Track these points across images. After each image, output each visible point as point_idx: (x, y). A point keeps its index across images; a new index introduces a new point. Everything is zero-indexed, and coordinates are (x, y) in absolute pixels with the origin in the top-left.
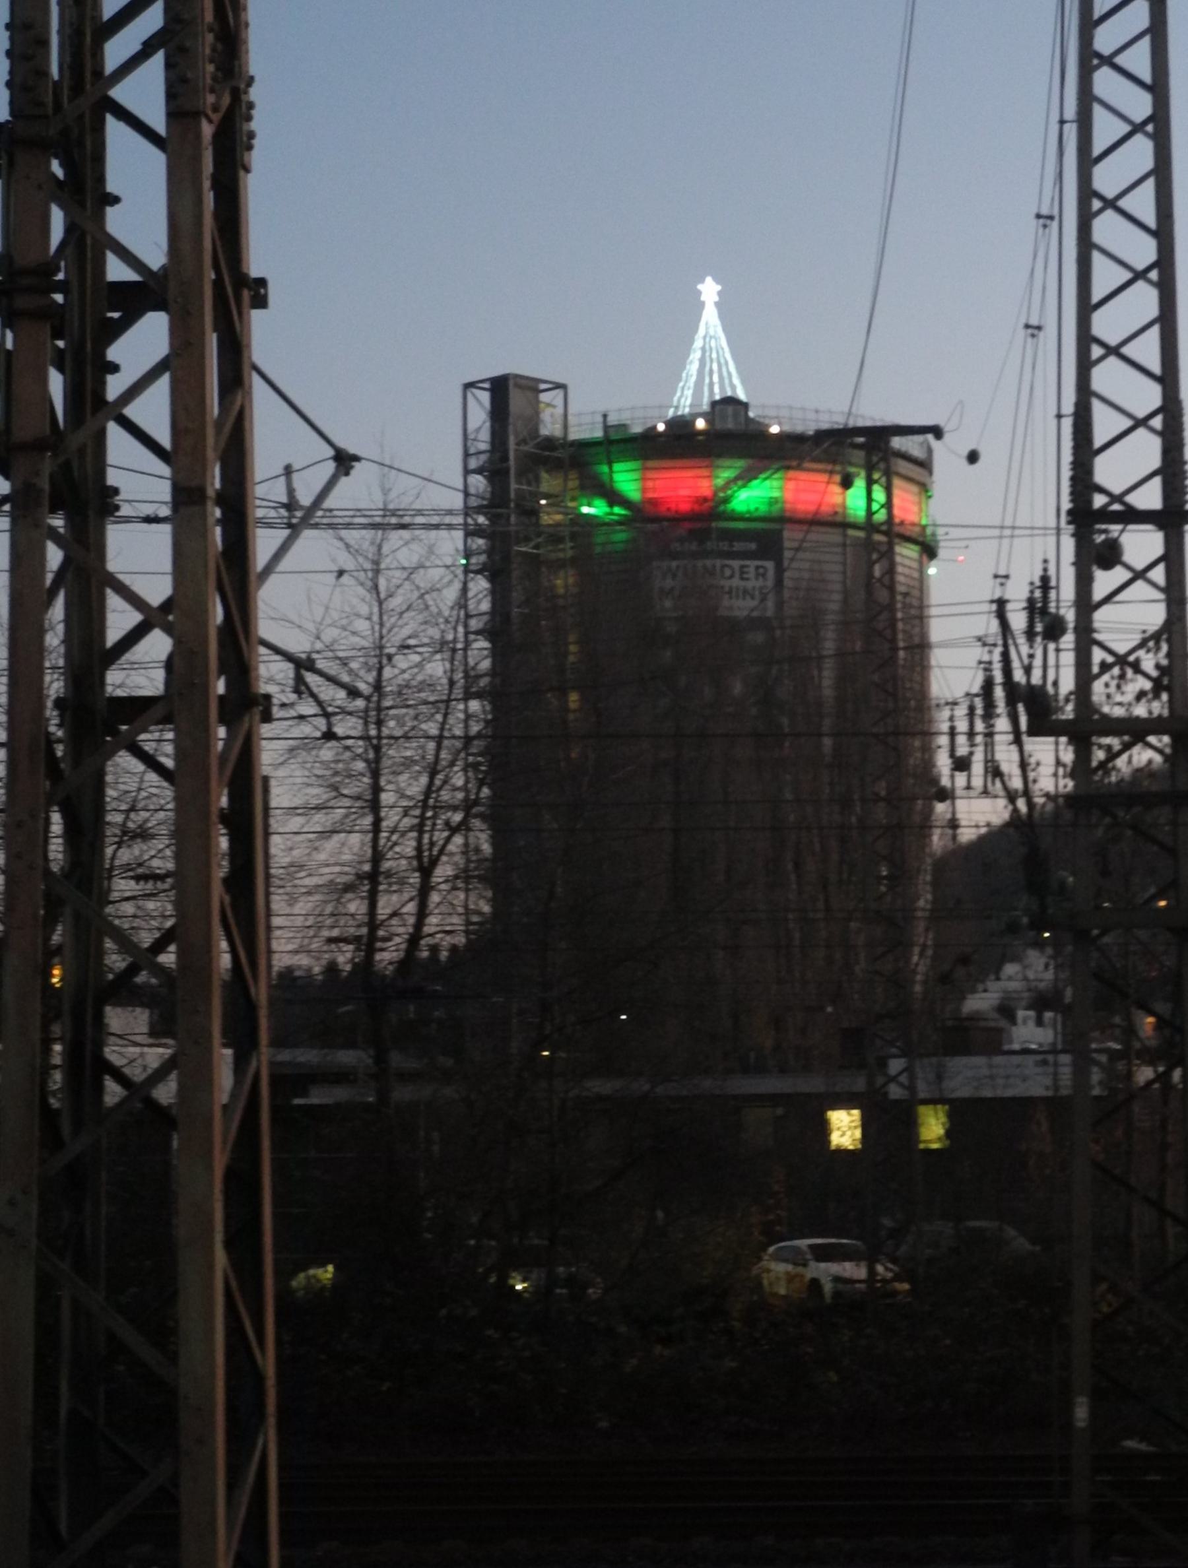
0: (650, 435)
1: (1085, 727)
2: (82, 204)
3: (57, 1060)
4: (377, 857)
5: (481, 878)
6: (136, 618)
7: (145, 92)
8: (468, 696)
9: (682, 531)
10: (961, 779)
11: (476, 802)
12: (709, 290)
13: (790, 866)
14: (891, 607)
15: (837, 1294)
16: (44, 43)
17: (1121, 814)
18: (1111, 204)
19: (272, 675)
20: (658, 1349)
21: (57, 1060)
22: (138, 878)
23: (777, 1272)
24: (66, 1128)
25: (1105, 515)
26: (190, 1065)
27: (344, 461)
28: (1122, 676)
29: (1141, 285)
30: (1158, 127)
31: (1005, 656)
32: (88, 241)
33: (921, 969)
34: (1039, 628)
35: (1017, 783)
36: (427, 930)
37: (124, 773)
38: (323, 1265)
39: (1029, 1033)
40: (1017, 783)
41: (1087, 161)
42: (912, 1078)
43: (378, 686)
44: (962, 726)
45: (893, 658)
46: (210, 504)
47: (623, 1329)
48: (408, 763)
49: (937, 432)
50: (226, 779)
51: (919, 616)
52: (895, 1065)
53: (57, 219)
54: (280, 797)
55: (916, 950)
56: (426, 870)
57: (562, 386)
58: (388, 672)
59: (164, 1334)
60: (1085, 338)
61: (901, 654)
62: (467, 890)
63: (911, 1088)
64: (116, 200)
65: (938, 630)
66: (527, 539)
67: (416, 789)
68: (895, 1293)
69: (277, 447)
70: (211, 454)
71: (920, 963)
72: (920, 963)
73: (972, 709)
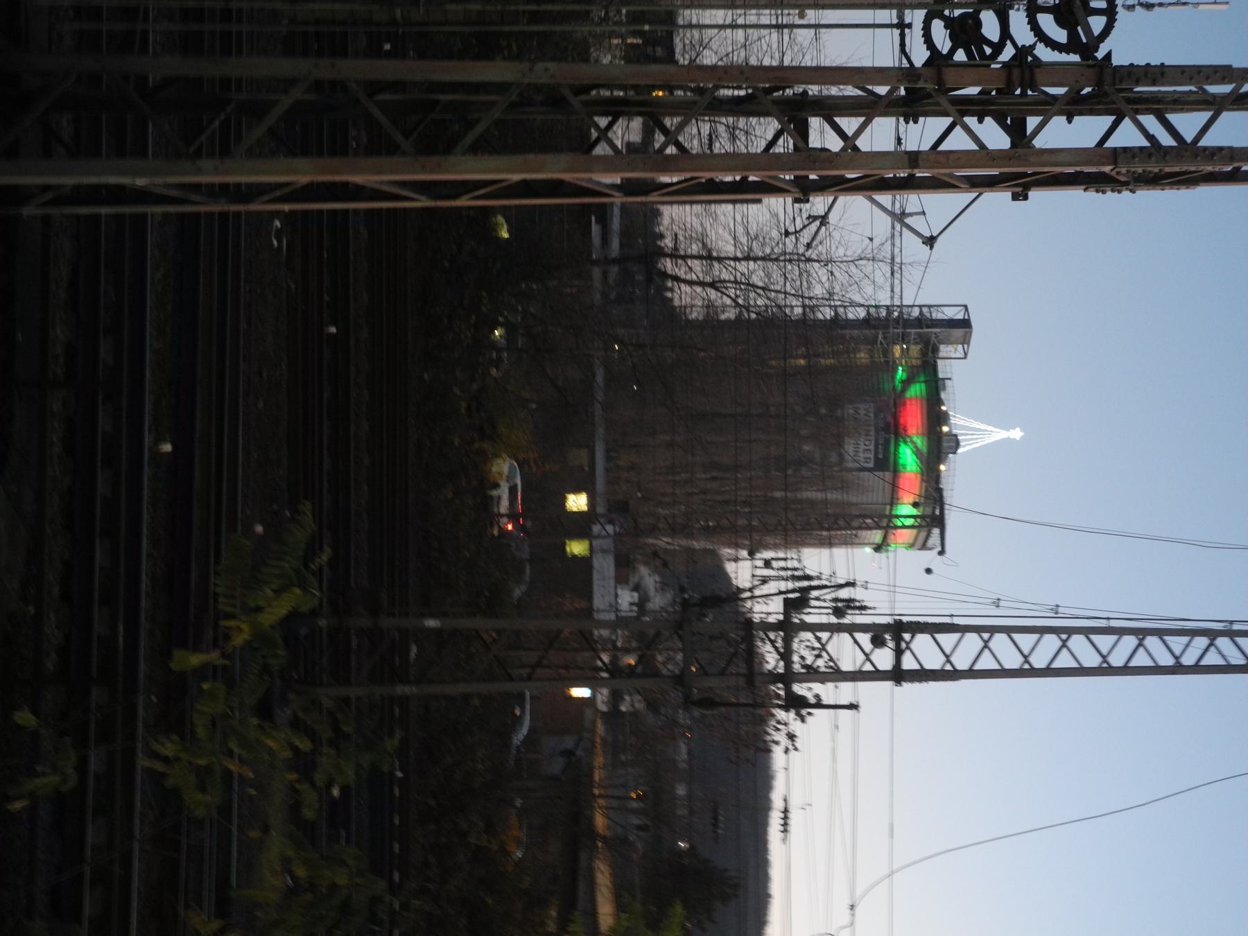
0: (940, 402)
1: (788, 628)
2: (1068, 104)
3: (616, 93)
4: (720, 259)
5: (708, 314)
6: (850, 133)
7: (1127, 136)
8: (804, 306)
9: (890, 419)
10: (760, 563)
11: (748, 311)
12: (1016, 434)
13: (714, 474)
14: (851, 528)
15: (492, 498)
16: (1154, 84)
17: (743, 647)
18: (1064, 645)
19: (818, 204)
20: (464, 404)
21: (616, 93)
22: (710, 135)
23: (503, 467)
24: (583, 97)
25: (898, 639)
26: (608, 165)
27: (930, 241)
28: (813, 649)
29: (1021, 659)
30: (1106, 670)
31: (825, 587)
32: (1048, 108)
33: (660, 543)
34: (840, 605)
35: (757, 592)
36: (683, 286)
37: (770, 126)
38: (509, 231)
39: (626, 598)
40: (757, 592)
41: (1160, 633)
42: (604, 537)
43: (809, 260)
44: (790, 564)
45: (823, 529)
46: (909, 171)
47: (475, 386)
48: (768, 276)
49: (942, 553)
50: (767, 180)
51: (847, 542)
52: (610, 528)
53: (1060, 91)
54: (753, 208)
55: (669, 540)
56: (712, 285)
57: (965, 358)
58: (816, 265)
59: (481, 147)
60: (993, 630)
61: (825, 533)
62: (702, 307)
63: (598, 537)
64: (1070, 122)
65: (839, 553)
66: (885, 338)
67: (755, 279)
68: (492, 527)
69: (935, 207)
70: (936, 171)
71: (663, 542)
72: (663, 542)
73: (796, 569)
